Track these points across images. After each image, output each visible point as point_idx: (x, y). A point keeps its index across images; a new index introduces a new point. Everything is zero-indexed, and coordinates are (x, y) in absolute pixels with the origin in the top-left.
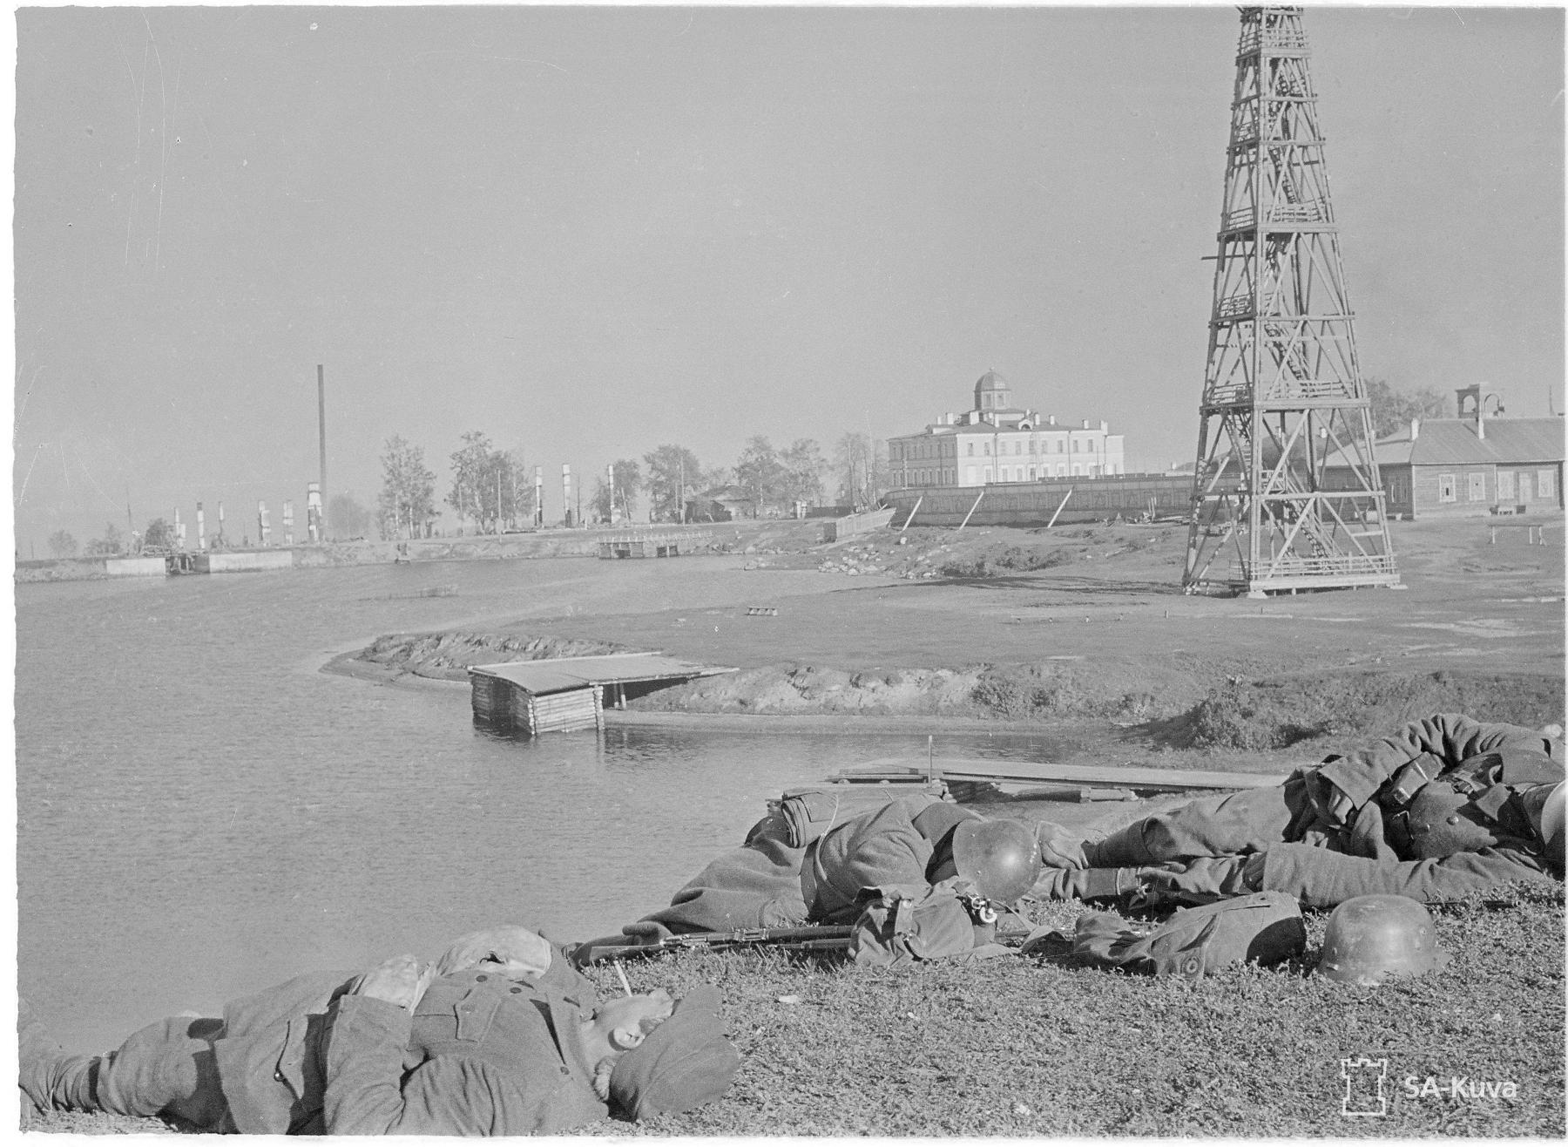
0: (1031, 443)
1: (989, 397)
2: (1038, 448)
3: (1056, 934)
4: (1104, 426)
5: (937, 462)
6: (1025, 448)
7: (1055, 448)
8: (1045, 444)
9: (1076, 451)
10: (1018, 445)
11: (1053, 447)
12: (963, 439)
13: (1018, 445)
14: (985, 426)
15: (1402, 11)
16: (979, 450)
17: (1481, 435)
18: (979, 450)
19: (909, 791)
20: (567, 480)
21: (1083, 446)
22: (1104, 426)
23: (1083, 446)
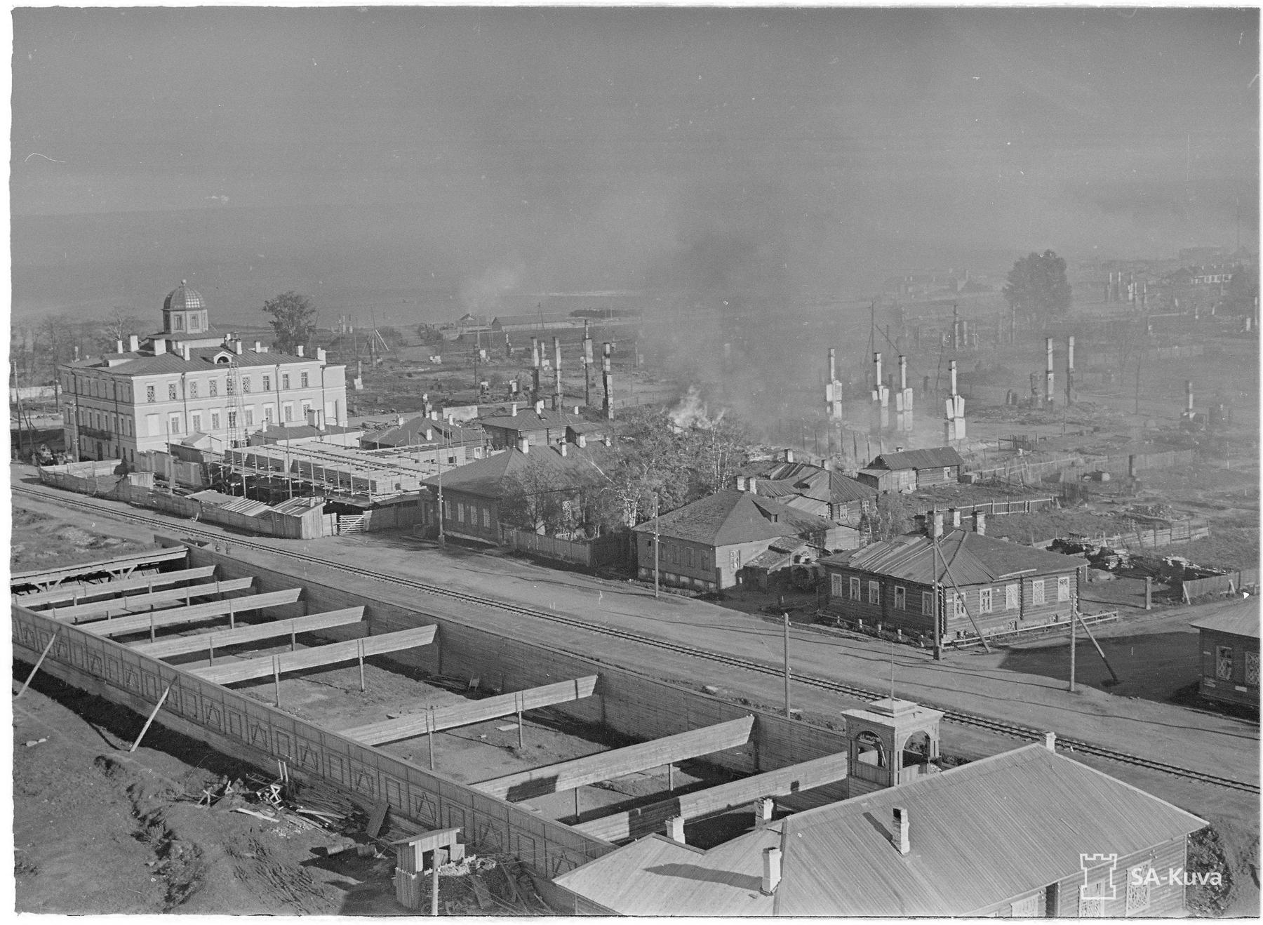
0: (229, 382)
1: (180, 318)
2: (239, 388)
3: (511, 789)
4: (322, 354)
5: (112, 406)
6: (222, 389)
7: (261, 386)
8: (246, 382)
9: (195, 396)
10: (213, 383)
11: (257, 384)
12: (140, 383)
13: (213, 383)
14: (173, 362)
15: (1129, 11)
16: (162, 393)
17: (905, 846)
18: (162, 393)
19: (482, 625)
20: (1051, 376)
21: (296, 381)
22: (322, 354)
23: (296, 381)
